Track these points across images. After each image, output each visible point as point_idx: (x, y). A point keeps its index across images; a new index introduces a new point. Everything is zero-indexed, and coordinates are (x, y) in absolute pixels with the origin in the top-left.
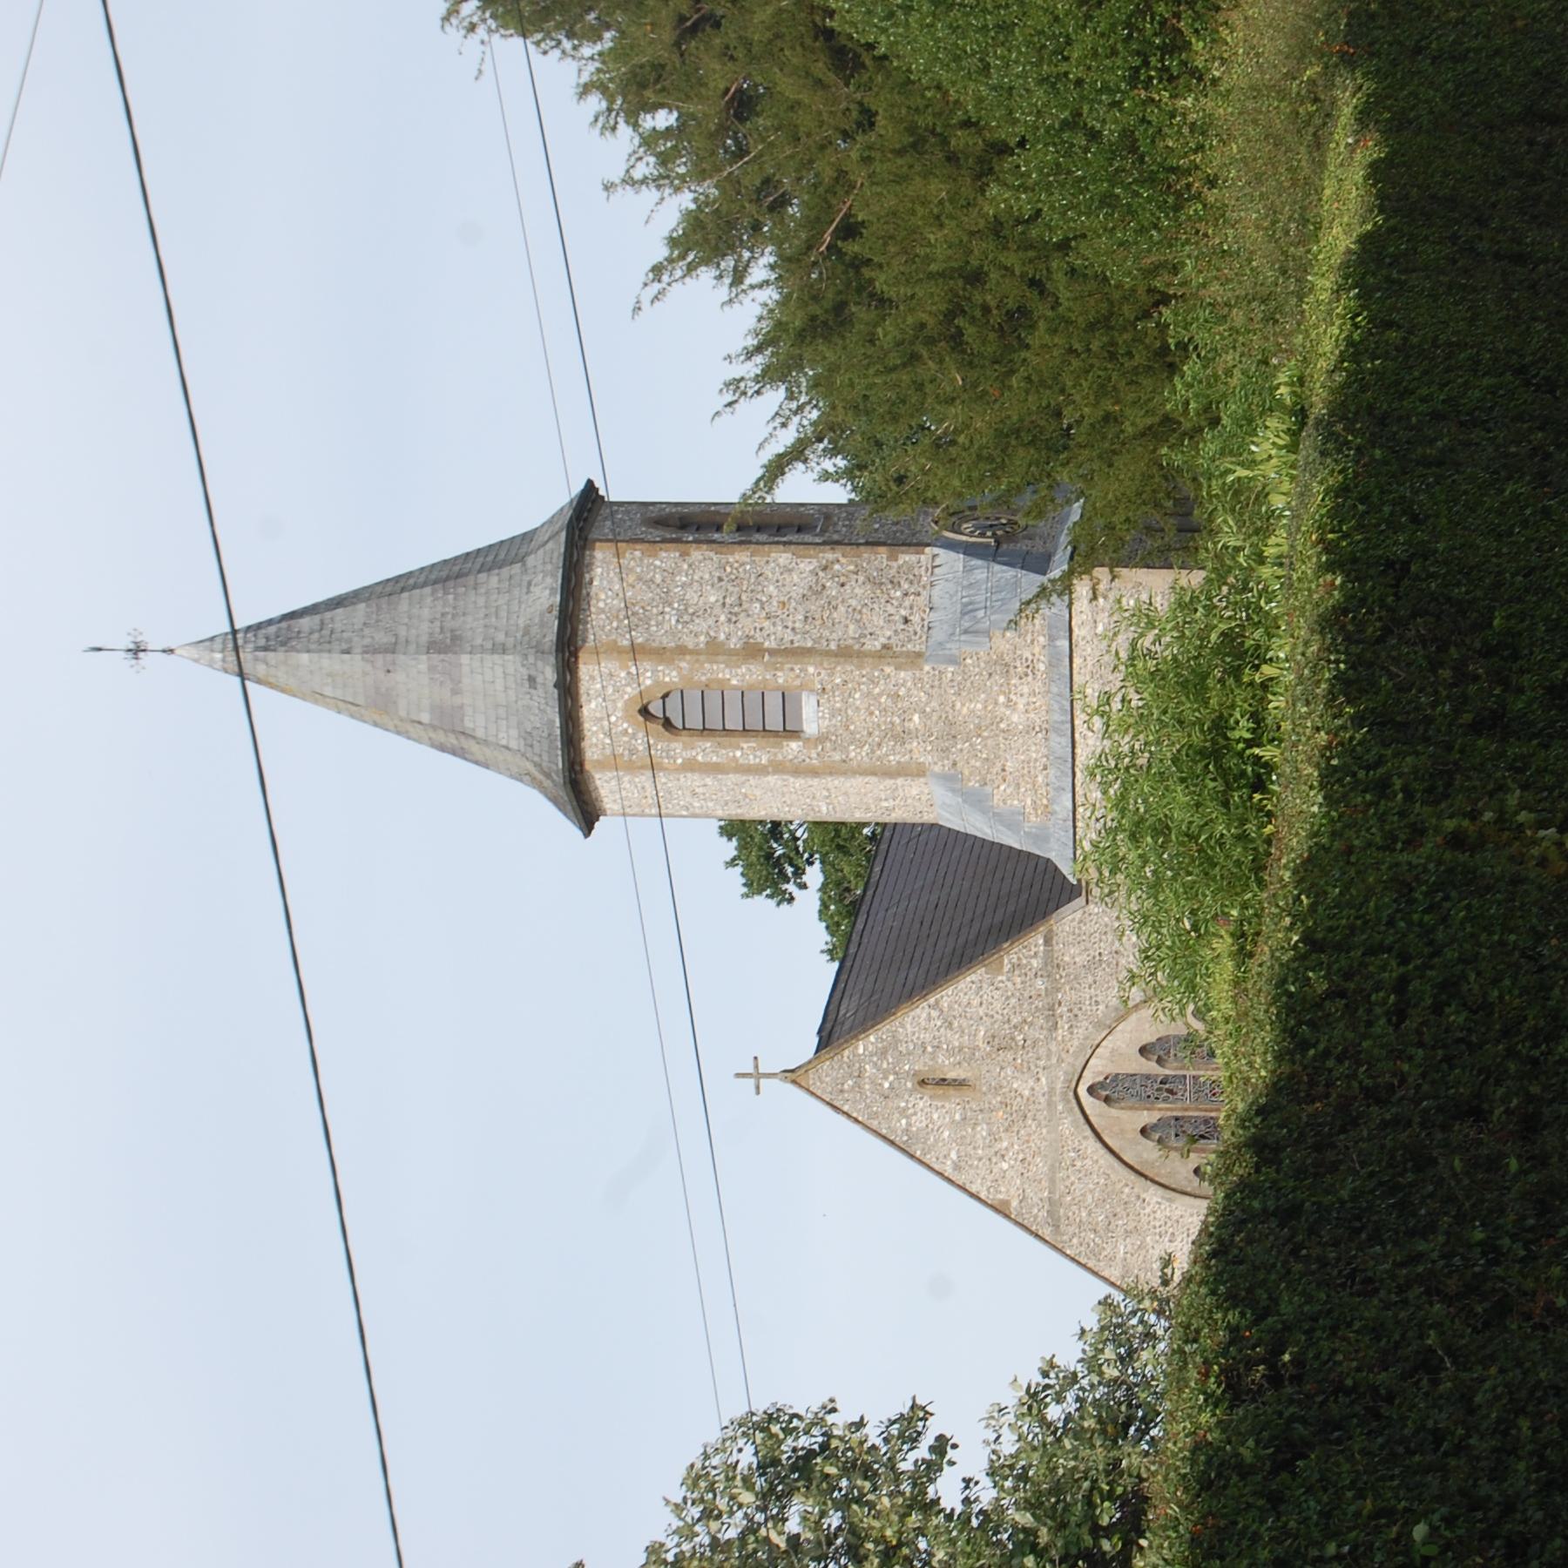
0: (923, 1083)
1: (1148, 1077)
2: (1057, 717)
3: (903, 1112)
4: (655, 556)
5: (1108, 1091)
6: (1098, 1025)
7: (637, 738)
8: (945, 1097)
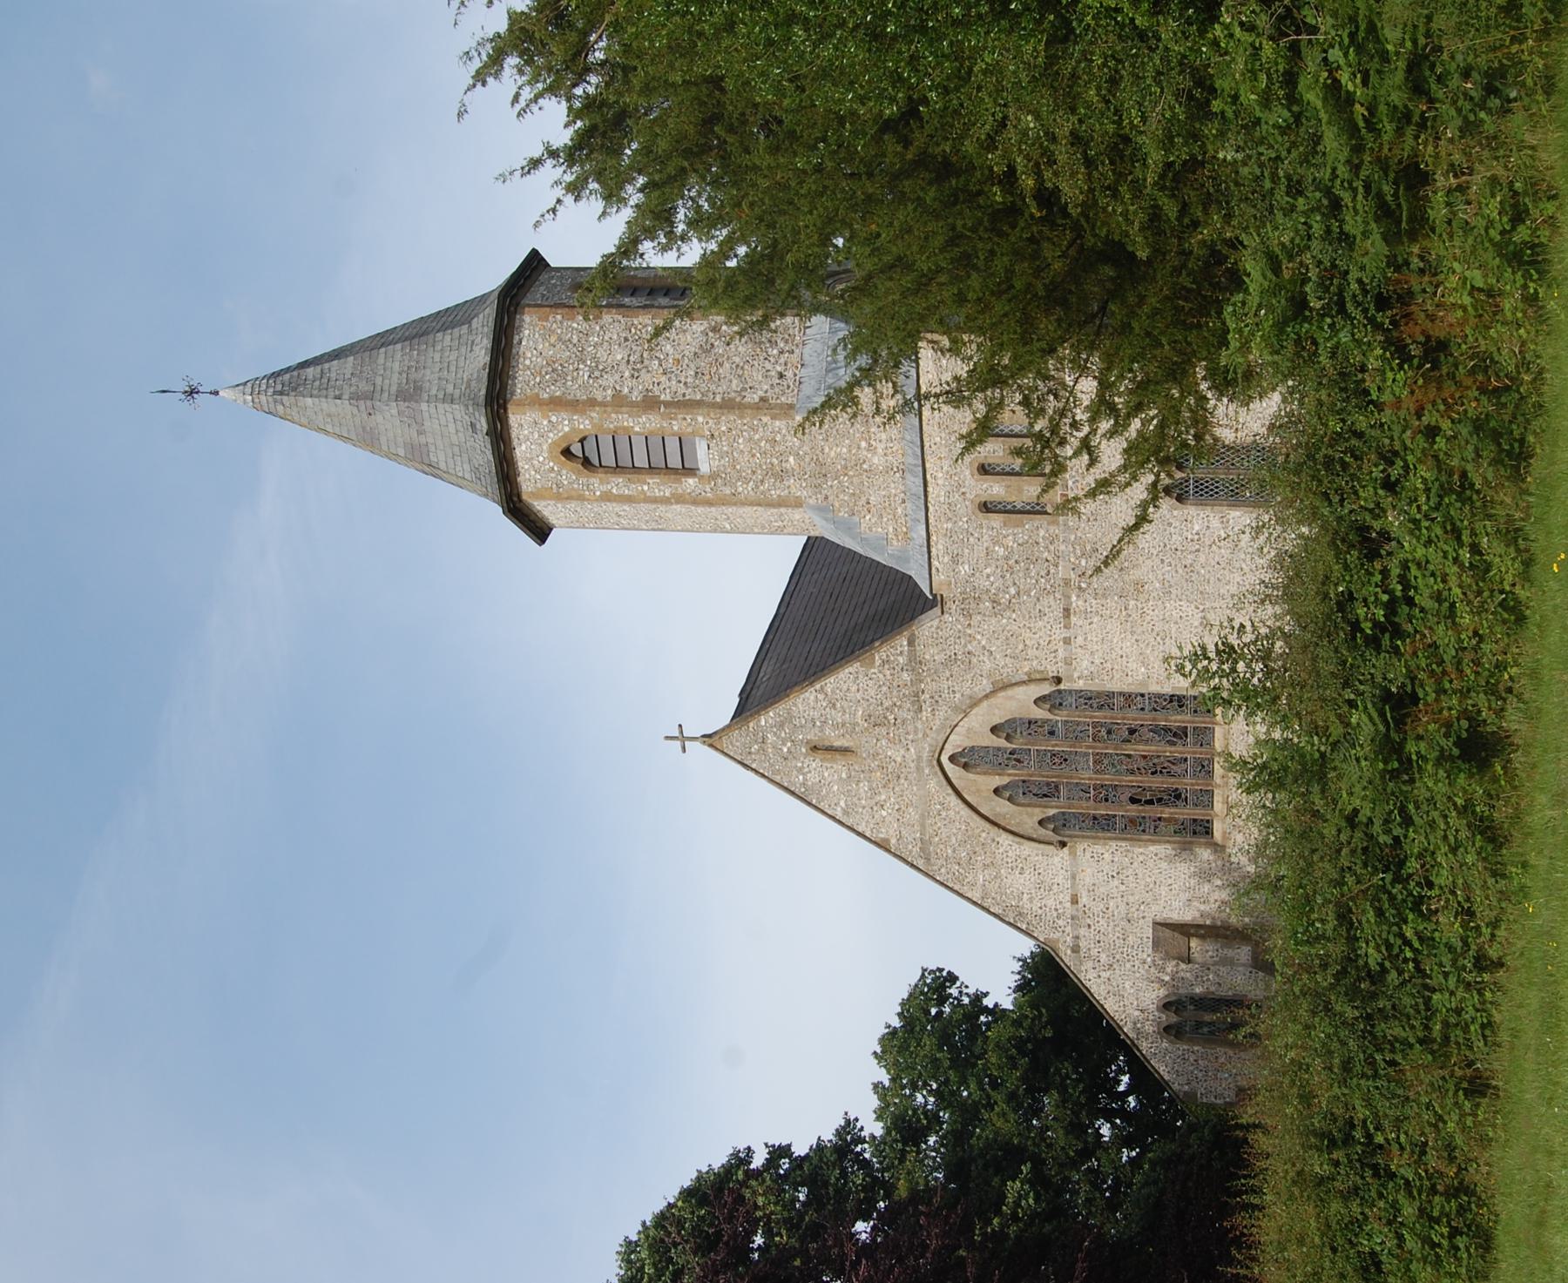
0: (815, 748)
1: (999, 749)
2: (911, 460)
3: (800, 770)
4: (573, 319)
5: (967, 759)
6: (956, 709)
7: (569, 475)
8: (833, 760)
